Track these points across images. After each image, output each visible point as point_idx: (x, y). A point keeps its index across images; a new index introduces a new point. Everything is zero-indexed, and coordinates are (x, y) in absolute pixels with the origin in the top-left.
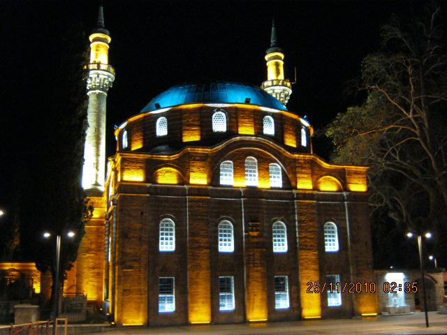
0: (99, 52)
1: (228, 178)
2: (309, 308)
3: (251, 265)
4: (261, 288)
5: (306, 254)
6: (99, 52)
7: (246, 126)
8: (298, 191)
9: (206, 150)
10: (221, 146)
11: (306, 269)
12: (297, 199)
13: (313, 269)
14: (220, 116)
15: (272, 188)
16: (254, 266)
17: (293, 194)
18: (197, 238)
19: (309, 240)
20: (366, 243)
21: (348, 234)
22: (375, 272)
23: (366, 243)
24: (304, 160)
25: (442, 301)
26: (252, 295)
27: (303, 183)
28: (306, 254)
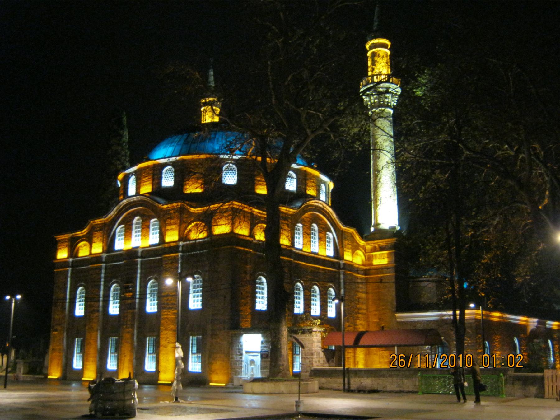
0: (380, 59)
1: (120, 244)
2: (165, 373)
3: (125, 327)
4: (130, 349)
5: (166, 313)
6: (380, 59)
7: (146, 185)
8: (344, 262)
9: (101, 219)
10: (112, 213)
11: (166, 329)
12: (344, 269)
13: (172, 330)
14: (229, 169)
15: (151, 246)
16: (126, 328)
17: (339, 264)
18: (93, 303)
19: (170, 298)
20: (225, 297)
21: (139, 275)
22: (231, 332)
23: (225, 297)
24: (174, 209)
25: (308, 374)
26: (123, 355)
27: (170, 236)
28: (166, 313)
